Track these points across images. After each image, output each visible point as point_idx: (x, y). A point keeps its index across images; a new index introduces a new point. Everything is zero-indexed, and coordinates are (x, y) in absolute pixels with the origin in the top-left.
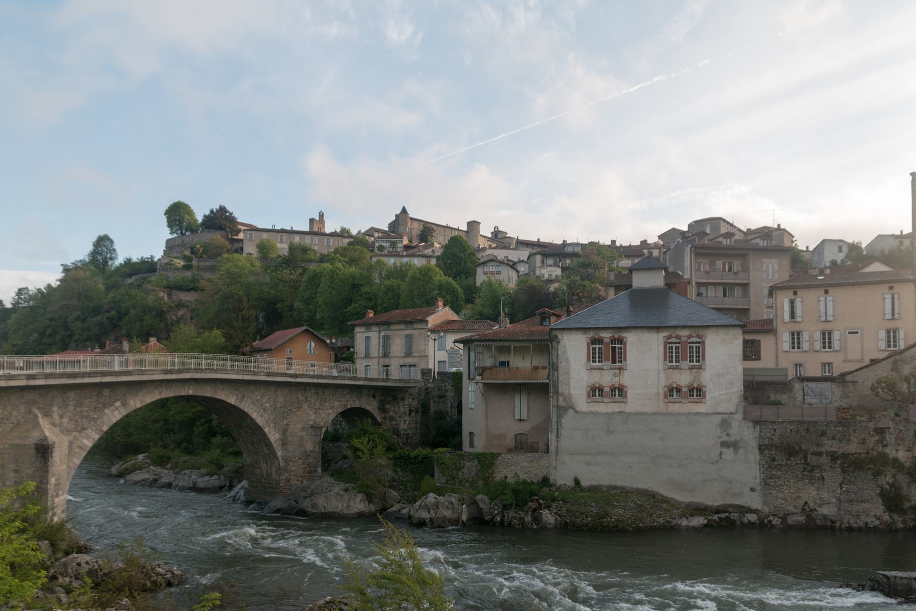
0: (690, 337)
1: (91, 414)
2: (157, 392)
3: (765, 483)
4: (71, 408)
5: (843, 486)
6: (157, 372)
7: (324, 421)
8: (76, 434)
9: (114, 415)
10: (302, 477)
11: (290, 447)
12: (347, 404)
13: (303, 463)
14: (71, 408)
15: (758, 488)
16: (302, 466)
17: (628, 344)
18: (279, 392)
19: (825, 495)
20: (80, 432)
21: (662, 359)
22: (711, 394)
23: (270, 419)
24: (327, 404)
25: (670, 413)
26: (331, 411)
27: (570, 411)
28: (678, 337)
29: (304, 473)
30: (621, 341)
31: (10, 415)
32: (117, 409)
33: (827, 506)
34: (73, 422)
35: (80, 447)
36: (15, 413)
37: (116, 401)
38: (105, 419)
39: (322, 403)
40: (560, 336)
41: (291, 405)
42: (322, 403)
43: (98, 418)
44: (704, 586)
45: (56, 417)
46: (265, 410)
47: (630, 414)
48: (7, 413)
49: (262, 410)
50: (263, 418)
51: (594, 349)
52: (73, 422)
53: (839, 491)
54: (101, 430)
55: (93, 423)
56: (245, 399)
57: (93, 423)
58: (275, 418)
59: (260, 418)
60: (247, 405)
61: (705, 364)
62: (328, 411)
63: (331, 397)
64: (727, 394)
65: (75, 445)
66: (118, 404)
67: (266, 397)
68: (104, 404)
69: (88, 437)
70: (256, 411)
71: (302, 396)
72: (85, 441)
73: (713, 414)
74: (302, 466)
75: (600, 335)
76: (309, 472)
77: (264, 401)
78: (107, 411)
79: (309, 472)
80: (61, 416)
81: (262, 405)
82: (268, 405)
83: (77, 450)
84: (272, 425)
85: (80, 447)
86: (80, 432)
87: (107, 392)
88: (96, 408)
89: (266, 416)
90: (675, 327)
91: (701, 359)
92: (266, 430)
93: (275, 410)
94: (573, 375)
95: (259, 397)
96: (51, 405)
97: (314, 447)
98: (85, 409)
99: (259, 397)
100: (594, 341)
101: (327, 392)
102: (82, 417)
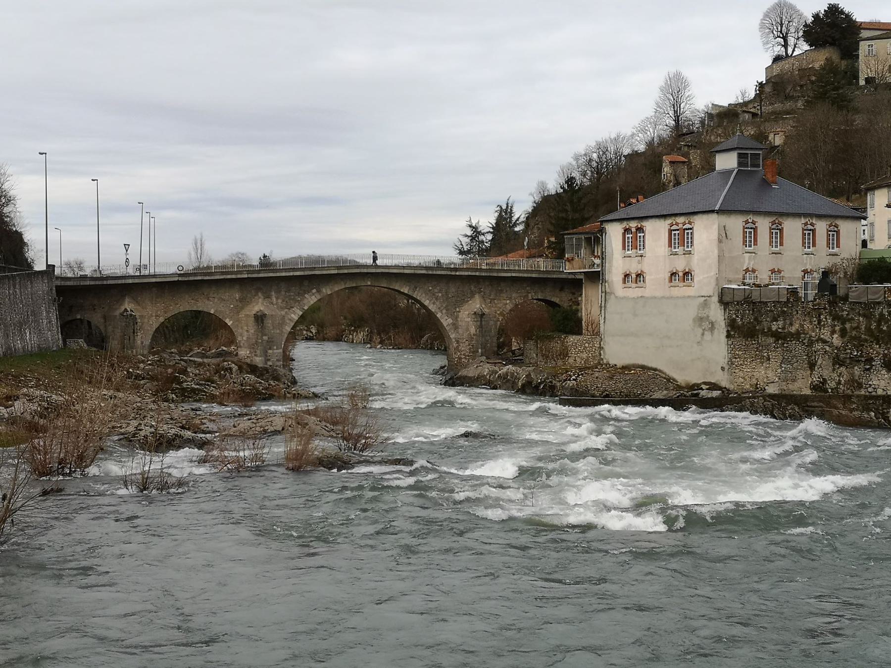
0: (684, 224)
1: (297, 297)
2: (342, 283)
3: (731, 363)
4: (283, 293)
5: (783, 365)
6: (333, 268)
7: (501, 310)
8: (287, 310)
9: (311, 299)
10: (468, 356)
11: (460, 331)
12: (528, 295)
13: (469, 345)
14: (283, 293)
15: (727, 368)
16: (468, 347)
17: (647, 232)
18: (450, 284)
19: (770, 374)
20: (289, 309)
21: (667, 246)
22: (699, 276)
23: (442, 306)
24: (504, 295)
25: (672, 297)
26: (508, 301)
27: (612, 296)
28: (677, 224)
29: (470, 353)
30: (640, 229)
31: (247, 296)
32: (313, 294)
33: (772, 384)
34: (285, 303)
35: (290, 320)
36: (249, 295)
37: (313, 289)
38: (305, 301)
39: (498, 294)
40: (606, 227)
41: (464, 295)
42: (498, 294)
43: (301, 300)
44: (489, 405)
45: (274, 299)
46: (437, 299)
47: (647, 298)
48: (244, 295)
49: (434, 299)
50: (435, 306)
51: (628, 238)
52: (285, 303)
53: (779, 371)
54: (304, 309)
55: (297, 304)
56: (418, 289)
57: (297, 304)
58: (447, 306)
59: (432, 305)
60: (420, 294)
61: (694, 249)
62: (505, 301)
63: (508, 289)
64: (708, 277)
65: (286, 318)
66: (314, 291)
67: (438, 288)
68: (304, 290)
69: (294, 313)
70: (428, 299)
71: (475, 287)
72: (293, 315)
73: (699, 297)
74: (468, 347)
75: (630, 225)
76: (473, 352)
77: (436, 291)
78: (306, 295)
79: (473, 352)
80: (277, 298)
81: (434, 295)
82: (440, 295)
83: (288, 321)
84: (444, 311)
85: (290, 320)
86: (289, 309)
87: (306, 283)
88: (299, 294)
89: (438, 303)
90: (676, 215)
91: (779, 244)
92: (439, 315)
93: (447, 299)
94: (615, 263)
95: (430, 288)
96: (271, 291)
97: (476, 330)
98: (292, 294)
99: (430, 288)
100: (627, 230)
101: (502, 284)
102: (290, 299)
